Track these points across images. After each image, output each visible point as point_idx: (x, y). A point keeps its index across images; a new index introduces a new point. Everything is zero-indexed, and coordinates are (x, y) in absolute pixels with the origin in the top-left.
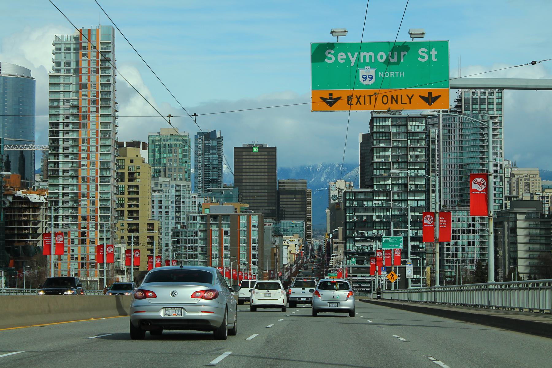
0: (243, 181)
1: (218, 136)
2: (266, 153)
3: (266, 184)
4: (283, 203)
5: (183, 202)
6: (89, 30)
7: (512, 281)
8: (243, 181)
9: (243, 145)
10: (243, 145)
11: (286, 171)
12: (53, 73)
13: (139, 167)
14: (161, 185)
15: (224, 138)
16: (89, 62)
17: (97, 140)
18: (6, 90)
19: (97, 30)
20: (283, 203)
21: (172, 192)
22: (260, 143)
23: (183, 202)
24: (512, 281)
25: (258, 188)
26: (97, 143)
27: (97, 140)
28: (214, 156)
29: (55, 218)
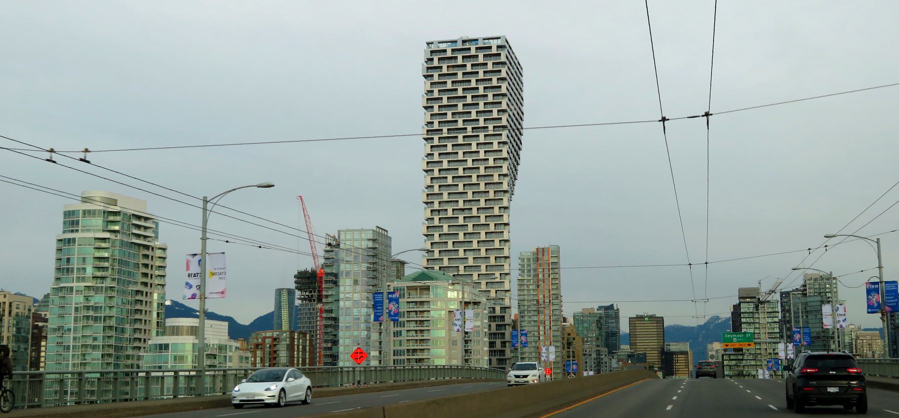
0: (638, 344)
1: (615, 308)
2: (655, 322)
3: (656, 346)
4: (223, 334)
5: (602, 363)
6: (543, 248)
7: (69, 363)
8: (638, 344)
9: (637, 315)
10: (637, 315)
11: (622, 332)
12: (520, 278)
13: (574, 339)
14: (586, 351)
15: (620, 310)
16: (544, 269)
17: (550, 322)
18: (124, 283)
19: (548, 248)
20: (223, 334)
21: (594, 355)
22: (650, 313)
23: (602, 363)
24: (69, 363)
25: (649, 349)
26: (550, 323)
27: (550, 322)
28: (612, 325)
29: (73, 340)
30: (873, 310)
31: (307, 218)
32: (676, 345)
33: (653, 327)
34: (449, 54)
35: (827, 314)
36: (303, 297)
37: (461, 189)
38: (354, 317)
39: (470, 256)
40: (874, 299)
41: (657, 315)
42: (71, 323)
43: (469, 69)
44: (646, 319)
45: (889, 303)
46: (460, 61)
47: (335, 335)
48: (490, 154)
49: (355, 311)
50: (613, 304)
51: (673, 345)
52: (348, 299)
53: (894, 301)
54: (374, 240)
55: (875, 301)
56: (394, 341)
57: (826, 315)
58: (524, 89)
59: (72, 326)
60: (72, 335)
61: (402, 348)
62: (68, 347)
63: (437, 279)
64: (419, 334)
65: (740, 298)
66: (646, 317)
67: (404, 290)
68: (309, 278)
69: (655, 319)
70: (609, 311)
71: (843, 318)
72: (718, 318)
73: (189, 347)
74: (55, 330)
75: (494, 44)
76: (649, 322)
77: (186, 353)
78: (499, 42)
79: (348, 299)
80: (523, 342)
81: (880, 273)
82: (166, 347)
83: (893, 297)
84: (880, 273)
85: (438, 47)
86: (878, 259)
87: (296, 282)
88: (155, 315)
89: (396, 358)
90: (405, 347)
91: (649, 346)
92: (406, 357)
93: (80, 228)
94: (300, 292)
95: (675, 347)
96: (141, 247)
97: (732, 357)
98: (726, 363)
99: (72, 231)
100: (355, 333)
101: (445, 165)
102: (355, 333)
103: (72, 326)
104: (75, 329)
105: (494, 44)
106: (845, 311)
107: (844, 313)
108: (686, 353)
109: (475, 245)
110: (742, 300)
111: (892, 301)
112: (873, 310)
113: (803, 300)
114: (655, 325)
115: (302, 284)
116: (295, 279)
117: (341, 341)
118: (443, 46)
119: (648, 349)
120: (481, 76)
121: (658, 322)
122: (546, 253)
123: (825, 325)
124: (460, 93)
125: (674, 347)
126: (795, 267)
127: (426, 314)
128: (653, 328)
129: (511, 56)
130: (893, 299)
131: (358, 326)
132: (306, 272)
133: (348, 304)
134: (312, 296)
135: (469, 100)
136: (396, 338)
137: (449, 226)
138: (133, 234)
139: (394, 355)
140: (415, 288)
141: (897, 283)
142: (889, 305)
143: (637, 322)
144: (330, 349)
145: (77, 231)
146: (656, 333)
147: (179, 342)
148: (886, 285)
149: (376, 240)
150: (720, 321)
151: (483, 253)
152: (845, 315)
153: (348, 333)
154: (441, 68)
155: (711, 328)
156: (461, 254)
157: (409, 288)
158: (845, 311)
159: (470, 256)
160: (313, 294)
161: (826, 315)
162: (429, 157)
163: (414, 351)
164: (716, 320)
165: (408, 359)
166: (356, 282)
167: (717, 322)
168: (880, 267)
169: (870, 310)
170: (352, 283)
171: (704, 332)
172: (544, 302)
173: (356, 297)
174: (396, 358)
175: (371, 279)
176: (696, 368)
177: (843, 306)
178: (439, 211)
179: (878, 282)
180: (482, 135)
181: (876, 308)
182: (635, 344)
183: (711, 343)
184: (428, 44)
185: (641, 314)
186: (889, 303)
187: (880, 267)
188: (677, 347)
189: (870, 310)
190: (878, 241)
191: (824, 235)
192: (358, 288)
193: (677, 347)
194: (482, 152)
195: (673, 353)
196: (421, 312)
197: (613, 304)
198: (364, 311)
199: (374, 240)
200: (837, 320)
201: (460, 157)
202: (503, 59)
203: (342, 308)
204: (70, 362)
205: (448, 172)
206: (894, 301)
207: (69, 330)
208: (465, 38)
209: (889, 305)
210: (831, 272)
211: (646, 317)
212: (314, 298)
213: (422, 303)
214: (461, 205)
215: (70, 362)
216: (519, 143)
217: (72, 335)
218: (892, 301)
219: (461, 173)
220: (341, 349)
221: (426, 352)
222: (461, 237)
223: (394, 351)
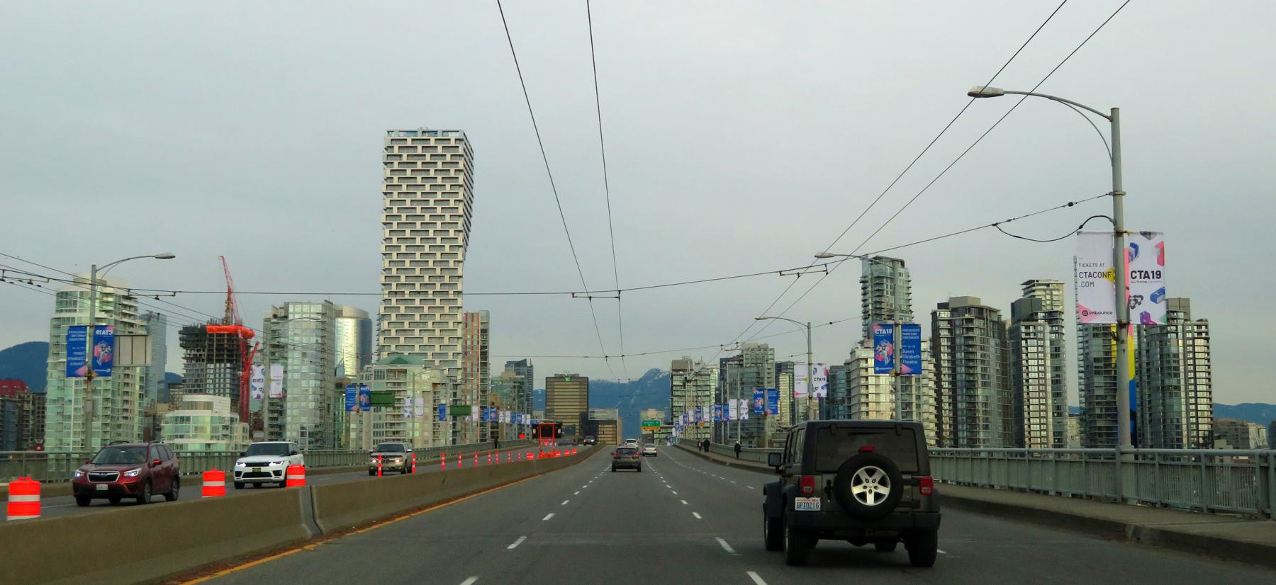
1: (528, 365)
2: (578, 383)
22: (572, 373)
30: (883, 369)
31: (229, 280)
32: (601, 412)
33: (575, 390)
34: (409, 143)
35: (1091, 270)
36: (188, 356)
37: (418, 272)
38: (303, 388)
39: (426, 336)
40: (885, 352)
41: (581, 375)
42: (71, 395)
43: (428, 159)
44: (567, 379)
45: (907, 360)
46: (419, 151)
47: (282, 406)
48: (447, 241)
49: (304, 383)
50: (526, 360)
51: (598, 412)
52: (295, 371)
53: (914, 357)
54: (323, 314)
55: (886, 355)
56: (374, 416)
57: (799, 380)
58: (475, 172)
59: (73, 398)
60: (73, 406)
61: (381, 422)
62: (69, 417)
63: (411, 363)
64: (396, 410)
65: (673, 370)
66: (567, 377)
67: (384, 372)
68: (197, 335)
69: (579, 380)
70: (521, 368)
71: (1152, 286)
72: (657, 371)
73: (208, 420)
74: (54, 401)
75: (453, 136)
76: (569, 383)
77: (206, 425)
78: (458, 135)
79: (295, 371)
80: (99, 363)
81: (1117, 208)
82: (188, 419)
83: (913, 352)
84: (1117, 208)
85: (399, 136)
86: (1111, 168)
87: (181, 339)
88: (137, 387)
89: (376, 430)
90: (383, 421)
91: (567, 412)
92: (385, 429)
93: (78, 308)
94: (185, 350)
95: (600, 415)
96: (127, 325)
97: (663, 431)
98: (656, 436)
99: (70, 311)
100: (303, 404)
101: (403, 250)
102: (303, 404)
103: (73, 398)
104: (76, 401)
105: (453, 136)
106: (1161, 261)
107: (1157, 268)
108: (613, 422)
109: (430, 326)
110: (674, 373)
111: (911, 357)
112: (883, 369)
113: (740, 370)
114: (578, 387)
115: (189, 341)
116: (179, 336)
117: (289, 412)
118: (402, 136)
119: (559, 417)
120: (439, 166)
121: (581, 384)
122: (475, 319)
123: (797, 394)
124: (419, 181)
125: (599, 414)
126: (821, 251)
127: (402, 394)
128: (574, 390)
129: (469, 152)
130: (913, 355)
131: (307, 398)
132: (193, 328)
133: (296, 376)
134: (201, 355)
135: (427, 189)
136: (376, 414)
137: (406, 307)
138: (123, 313)
139: (374, 428)
140: (394, 371)
141: (920, 328)
142: (908, 362)
143: (556, 383)
144: (276, 419)
145: (75, 311)
146: (578, 397)
147: (200, 415)
148: (904, 330)
149: (326, 314)
150: (661, 376)
151: (437, 334)
152: (1159, 275)
153: (295, 404)
154: (401, 156)
155: (649, 385)
156: (417, 333)
157: (388, 371)
158: (1161, 261)
159: (426, 336)
160: (201, 353)
161: (799, 380)
162: (387, 240)
163: (392, 425)
164: (655, 375)
165: (386, 431)
166: (304, 355)
167: (656, 378)
168: (1116, 194)
169: (877, 369)
170: (300, 356)
171: (638, 391)
172: (472, 371)
173: (305, 369)
174: (376, 430)
175: (320, 353)
176: (613, 457)
177: (1156, 240)
178: (396, 293)
179: (892, 325)
180: (439, 223)
181: (888, 366)
182: (552, 411)
183: (646, 409)
184: (388, 132)
185: (561, 372)
186: (907, 360)
187: (1116, 194)
188: (604, 414)
189: (877, 369)
190: (1113, 117)
191: (815, 254)
192: (307, 360)
193: (604, 414)
194: (439, 239)
195: (597, 423)
196: (398, 391)
197: (526, 360)
198: (312, 383)
199: (323, 314)
200: (1132, 292)
201: (418, 242)
202: (461, 151)
203: (290, 380)
204: (72, 430)
205: (405, 256)
206: (914, 357)
207: (70, 401)
208: (425, 129)
209: (908, 362)
210: (809, 323)
211: (567, 377)
212: (203, 357)
213: (399, 384)
214: (417, 288)
215: (72, 430)
216: (469, 225)
217: (73, 406)
218: (911, 357)
219: (418, 257)
220: (289, 419)
221: (402, 426)
222: (417, 318)
223: (374, 424)
